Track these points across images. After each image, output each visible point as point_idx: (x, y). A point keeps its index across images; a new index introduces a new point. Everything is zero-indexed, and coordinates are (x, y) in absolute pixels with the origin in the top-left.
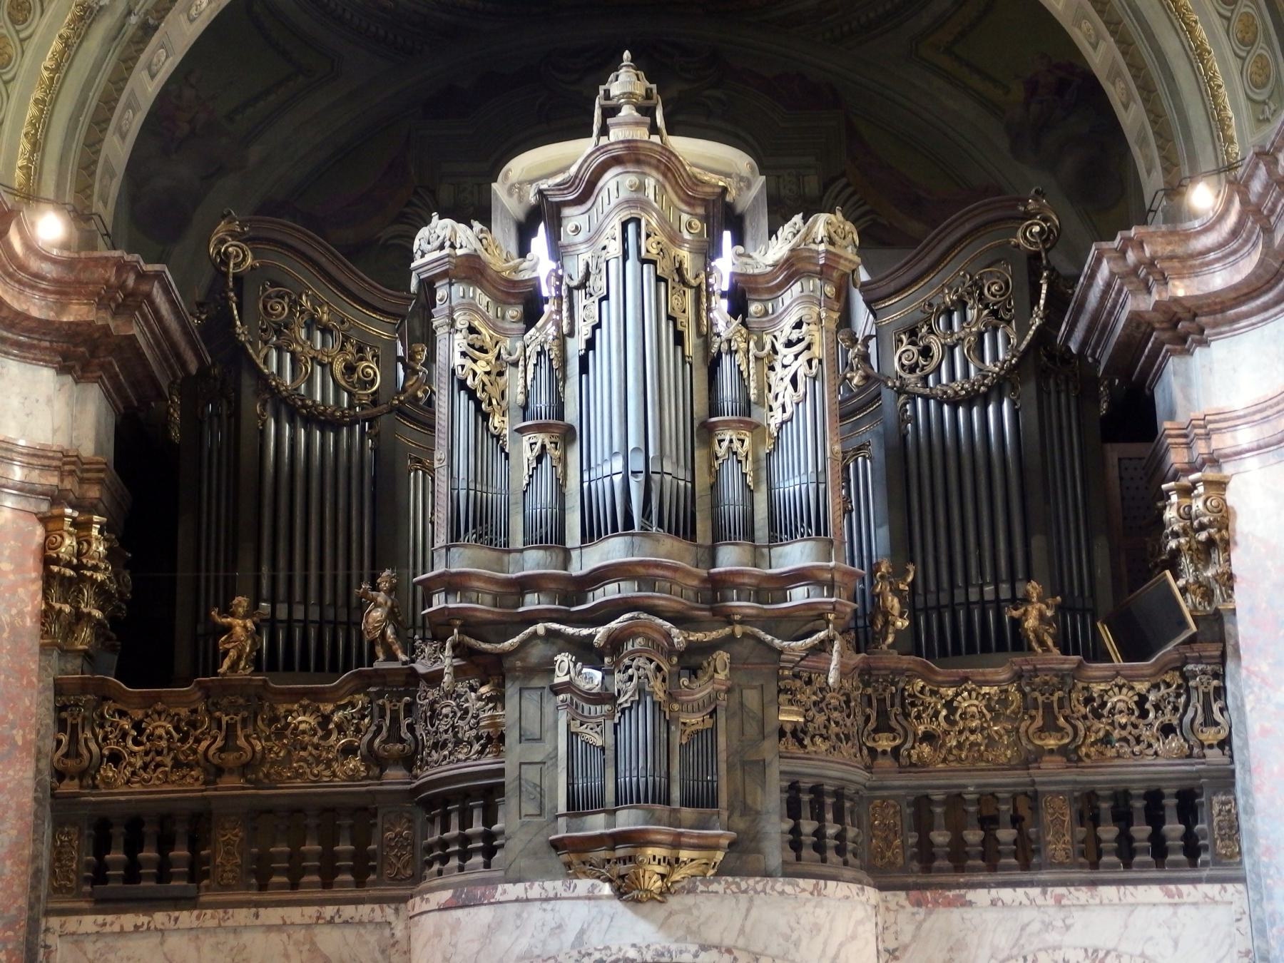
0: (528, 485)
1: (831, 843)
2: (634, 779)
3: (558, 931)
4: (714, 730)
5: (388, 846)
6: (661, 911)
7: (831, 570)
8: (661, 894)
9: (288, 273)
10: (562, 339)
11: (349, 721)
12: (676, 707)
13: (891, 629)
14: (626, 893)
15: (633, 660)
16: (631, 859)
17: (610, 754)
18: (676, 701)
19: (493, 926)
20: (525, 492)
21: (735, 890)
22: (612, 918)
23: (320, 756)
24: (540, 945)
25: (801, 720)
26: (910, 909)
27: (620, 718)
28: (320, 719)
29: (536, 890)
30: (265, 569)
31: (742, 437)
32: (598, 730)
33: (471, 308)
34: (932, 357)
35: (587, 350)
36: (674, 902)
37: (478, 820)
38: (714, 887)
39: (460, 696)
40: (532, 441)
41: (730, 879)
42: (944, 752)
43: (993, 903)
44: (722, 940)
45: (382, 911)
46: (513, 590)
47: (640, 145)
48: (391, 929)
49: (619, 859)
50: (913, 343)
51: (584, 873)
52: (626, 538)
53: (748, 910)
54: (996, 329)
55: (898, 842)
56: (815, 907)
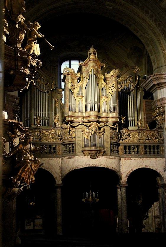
17: (90, 140)
30: (35, 112)
43: (134, 160)
50: (120, 85)
54: (131, 83)
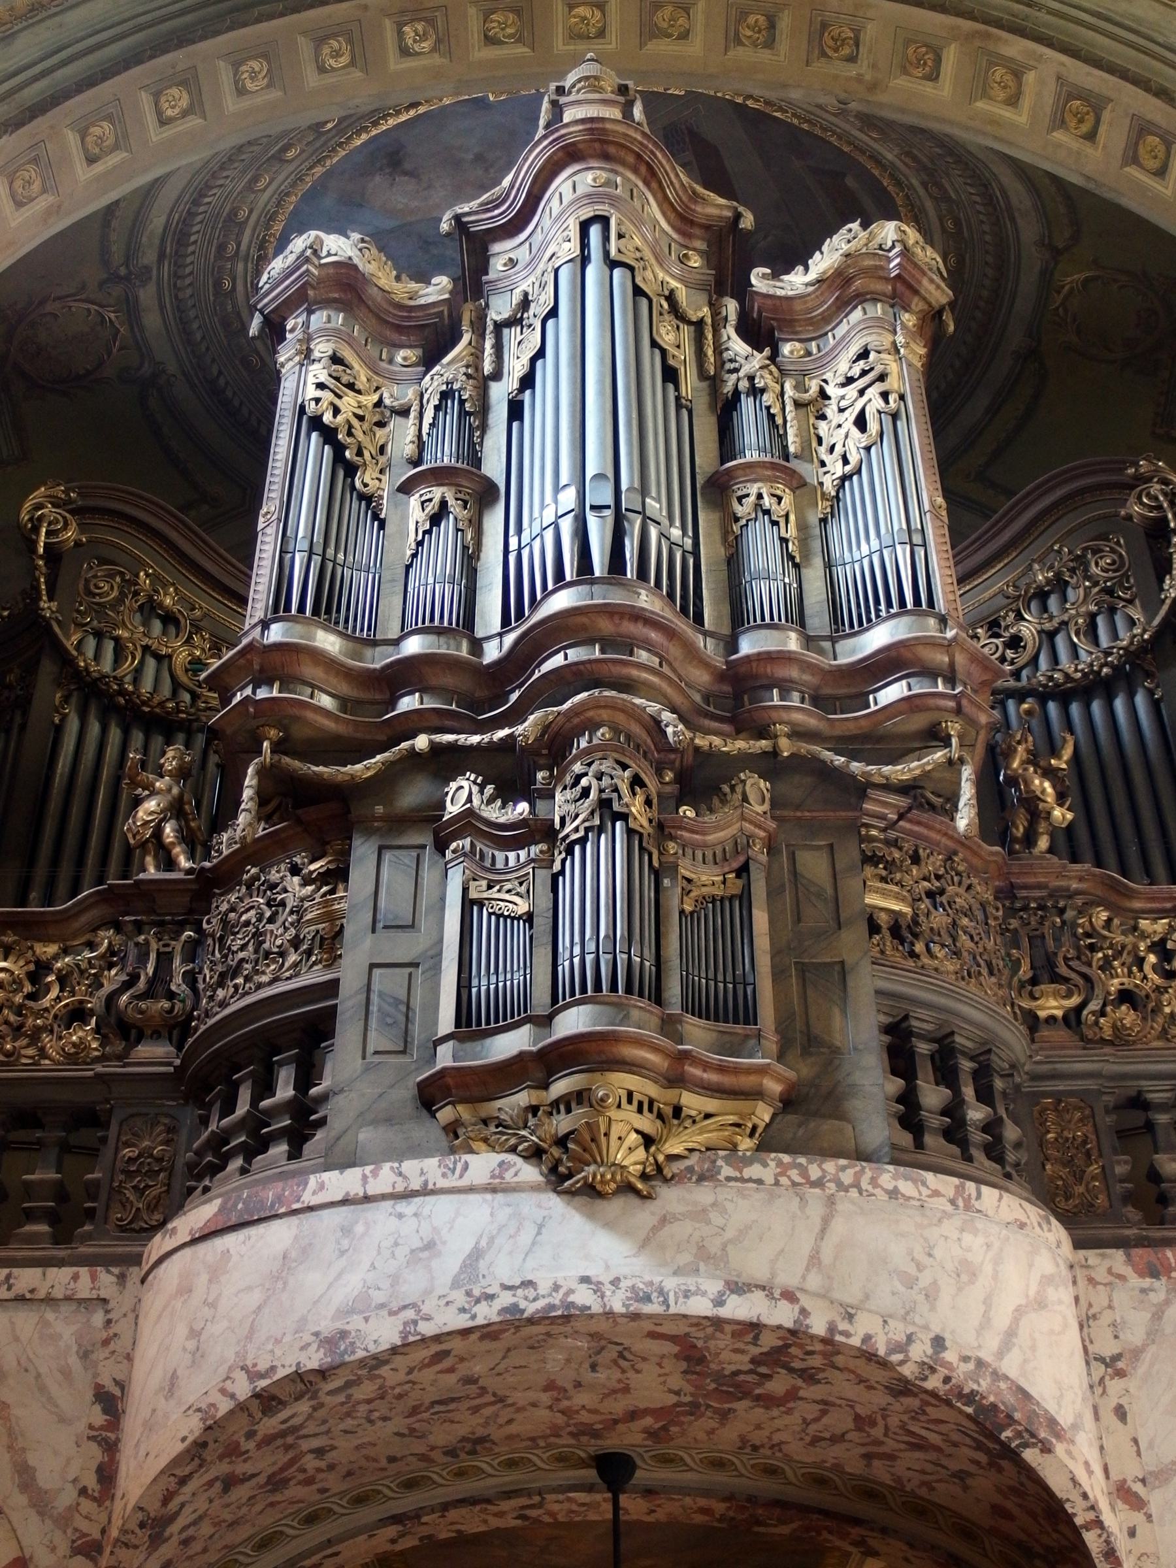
0: (414, 556)
1: (977, 1137)
2: (589, 958)
3: (425, 1254)
4: (745, 898)
5: (123, 1171)
6: (644, 1215)
7: (949, 646)
8: (644, 1176)
9: (123, 549)
10: (483, 383)
11: (82, 972)
12: (672, 847)
13: (1042, 827)
14: (570, 1176)
15: (589, 765)
16: (580, 1097)
17: (542, 923)
18: (672, 838)
19: (294, 1254)
20: (408, 567)
21: (798, 1179)
22: (540, 1227)
23: (22, 1026)
24: (385, 1284)
25: (907, 910)
26: (1135, 1281)
27: (563, 861)
28: (32, 967)
29: (385, 1179)
31: (778, 492)
32: (523, 889)
33: (335, 334)
34: (1024, 647)
35: (521, 390)
36: (670, 1197)
37: (287, 1083)
38: (755, 1171)
39: (272, 887)
40: (424, 498)
41: (786, 1158)
42: (1160, 1020)
44: (773, 1275)
45: (94, 1278)
46: (378, 697)
47: (608, 126)
48: (107, 1312)
49: (555, 1104)
51: (485, 1140)
52: (580, 588)
53: (826, 1221)
54: (1112, 610)
55: (1094, 1169)
56: (962, 1230)
